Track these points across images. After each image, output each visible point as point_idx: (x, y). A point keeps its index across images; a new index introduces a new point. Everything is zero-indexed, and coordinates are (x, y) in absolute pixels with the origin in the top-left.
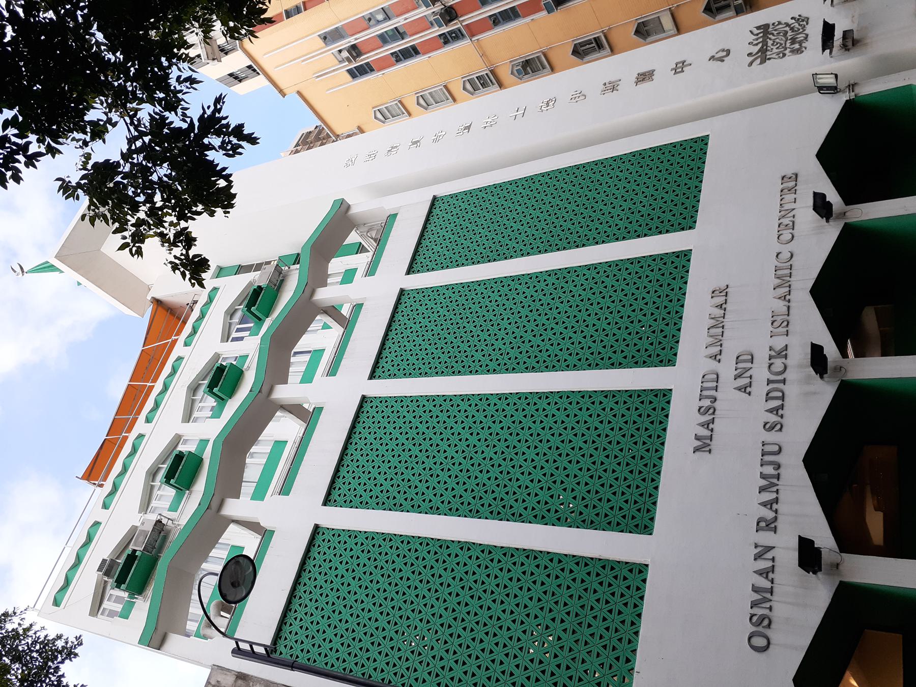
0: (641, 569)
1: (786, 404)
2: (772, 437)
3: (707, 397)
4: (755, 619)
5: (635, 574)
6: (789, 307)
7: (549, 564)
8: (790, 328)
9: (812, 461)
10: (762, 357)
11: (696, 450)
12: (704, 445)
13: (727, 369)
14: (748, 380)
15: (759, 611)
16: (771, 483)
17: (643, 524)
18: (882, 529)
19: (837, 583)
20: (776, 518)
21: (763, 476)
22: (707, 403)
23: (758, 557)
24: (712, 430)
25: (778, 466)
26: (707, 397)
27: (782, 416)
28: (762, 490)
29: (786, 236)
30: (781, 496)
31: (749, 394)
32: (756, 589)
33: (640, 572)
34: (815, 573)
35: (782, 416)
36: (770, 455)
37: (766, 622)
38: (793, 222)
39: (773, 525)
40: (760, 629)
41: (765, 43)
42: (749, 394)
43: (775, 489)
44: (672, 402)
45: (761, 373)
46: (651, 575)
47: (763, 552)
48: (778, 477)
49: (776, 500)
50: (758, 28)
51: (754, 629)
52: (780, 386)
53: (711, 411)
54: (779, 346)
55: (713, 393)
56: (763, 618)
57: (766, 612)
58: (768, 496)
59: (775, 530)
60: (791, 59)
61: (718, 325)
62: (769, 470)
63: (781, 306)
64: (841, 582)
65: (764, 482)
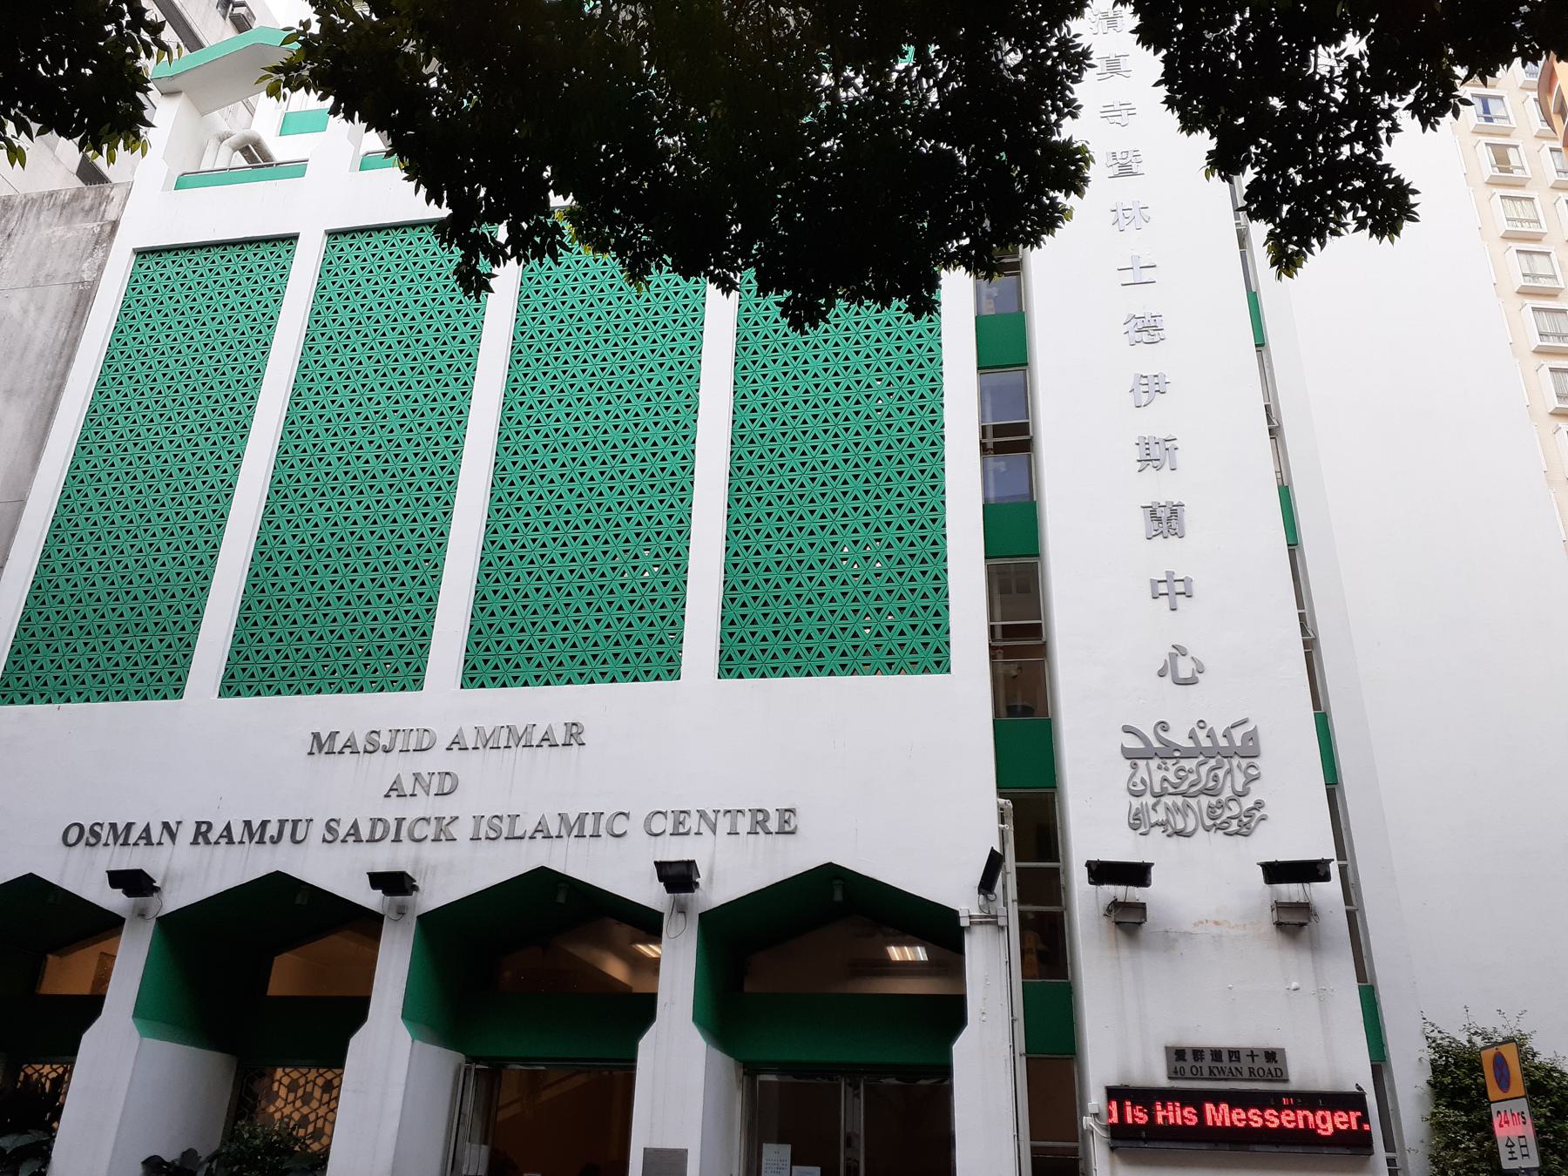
0: (941, 664)
2: (318, 830)
3: (393, 740)
4: (496, 821)
5: (661, 662)
6: (521, 838)
7: (929, 541)
8: (484, 843)
10: (446, 808)
11: (316, 736)
12: (321, 744)
13: (428, 763)
14: (408, 791)
15: (104, 833)
16: (256, 833)
17: (728, 667)
19: (659, 909)
20: (207, 842)
21: (581, 818)
22: (384, 740)
23: (166, 825)
24: (341, 752)
26: (393, 740)
27: (344, 841)
28: (248, 824)
29: (658, 824)
30: (236, 848)
31: (387, 796)
32: (129, 826)
33: (938, 663)
35: (344, 841)
36: (292, 831)
37: (93, 841)
38: (687, 834)
39: (759, 829)
40: (87, 834)
41: (1188, 755)
42: (387, 796)
43: (246, 839)
44: (12, 707)
45: (412, 809)
46: (665, 685)
48: (580, 836)
49: (359, 840)
50: (1252, 737)
51: (87, 829)
52: (392, 835)
54: (454, 830)
55: (399, 746)
56: (97, 836)
57: (103, 840)
59: (195, 842)
60: (1123, 805)
61: (519, 738)
62: (272, 830)
63: (526, 825)
64: (661, 915)
65: (255, 825)
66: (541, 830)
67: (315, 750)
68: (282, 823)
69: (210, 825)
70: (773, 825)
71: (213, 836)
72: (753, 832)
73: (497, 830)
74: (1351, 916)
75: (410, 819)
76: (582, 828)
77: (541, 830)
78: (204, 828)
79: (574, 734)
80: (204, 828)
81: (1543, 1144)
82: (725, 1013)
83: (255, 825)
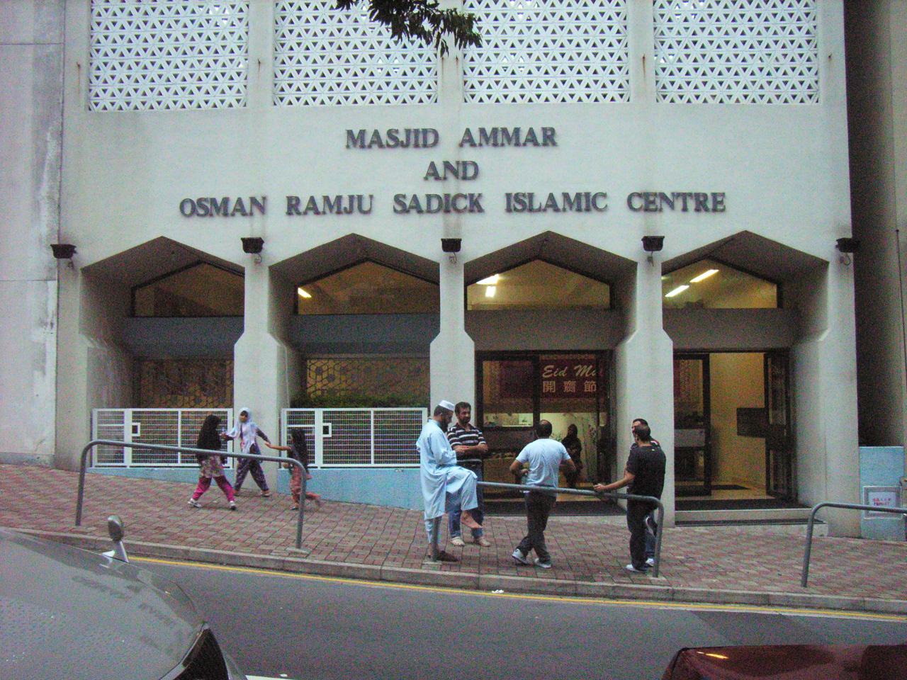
1: (694, 190)
9: (354, 241)
10: (468, 188)
11: (350, 133)
16: (335, 206)
18: (101, 258)
20: (299, 213)
21: (339, 198)
23: (253, 200)
25: (349, 212)
34: (837, 246)
36: (357, 205)
45: (453, 186)
47: (260, 205)
48: (339, 212)
53: (392, 143)
58: (320, 205)
63: (541, 200)
65: (332, 199)
66: (552, 204)
67: (351, 144)
68: (351, 198)
69: (298, 199)
70: (710, 205)
71: (302, 208)
72: (697, 210)
73: (519, 203)
74: (414, 275)
75: (593, 194)
76: (579, 204)
77: (552, 204)
78: (294, 202)
79: (549, 137)
80: (294, 202)
81: (576, 388)
82: (290, 323)
83: (332, 199)
